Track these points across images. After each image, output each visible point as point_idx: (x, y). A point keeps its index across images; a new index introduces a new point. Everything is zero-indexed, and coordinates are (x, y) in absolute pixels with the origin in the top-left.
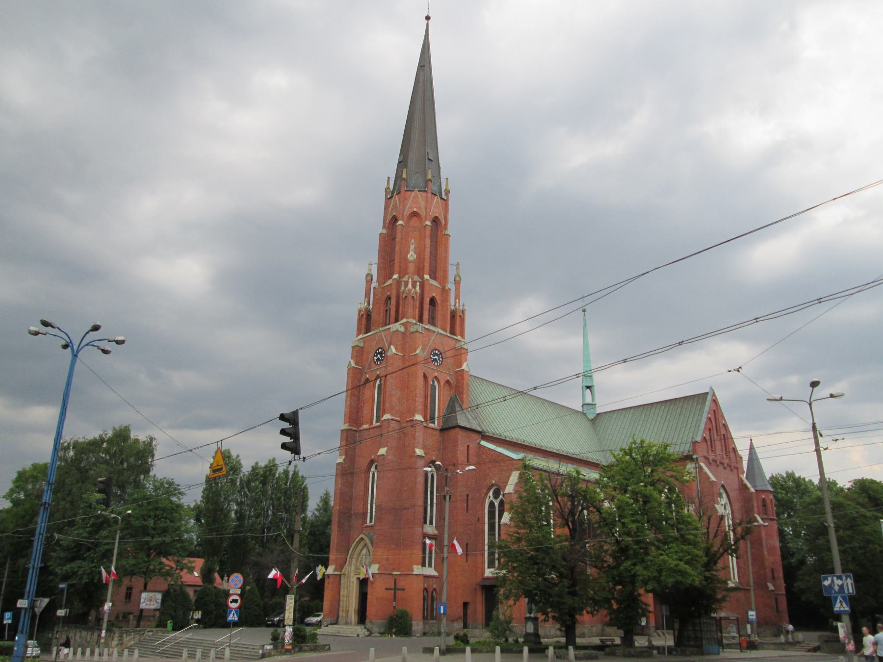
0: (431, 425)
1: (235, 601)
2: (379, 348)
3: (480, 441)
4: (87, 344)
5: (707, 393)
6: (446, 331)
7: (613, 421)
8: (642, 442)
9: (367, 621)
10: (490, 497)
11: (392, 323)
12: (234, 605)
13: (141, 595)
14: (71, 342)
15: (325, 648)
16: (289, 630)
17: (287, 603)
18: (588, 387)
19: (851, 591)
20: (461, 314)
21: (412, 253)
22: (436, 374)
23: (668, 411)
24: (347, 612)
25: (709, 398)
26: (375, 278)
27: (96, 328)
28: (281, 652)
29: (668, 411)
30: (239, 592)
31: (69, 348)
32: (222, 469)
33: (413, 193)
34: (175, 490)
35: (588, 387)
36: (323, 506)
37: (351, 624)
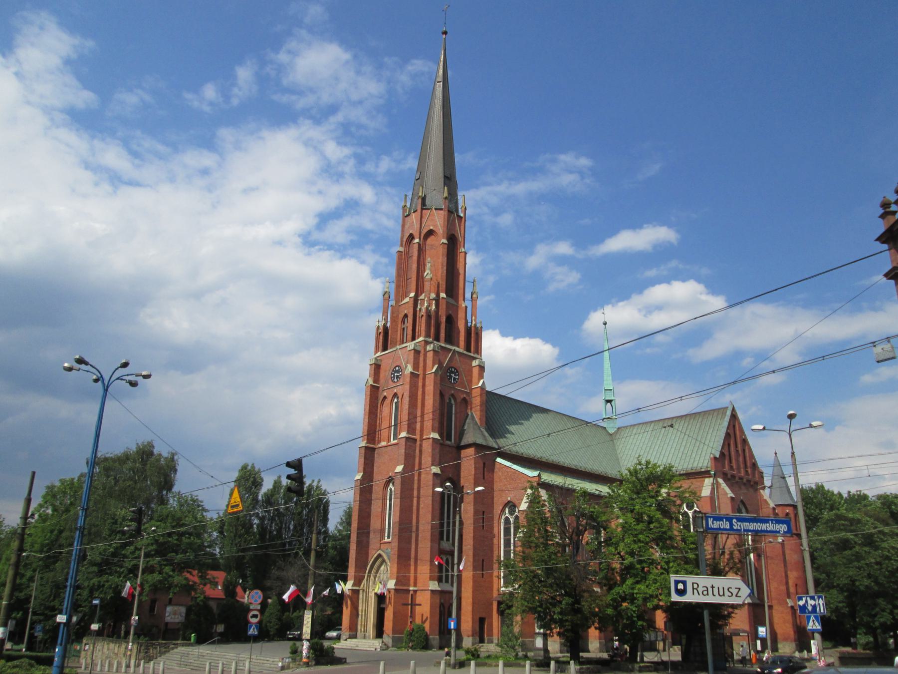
0: (448, 442)
1: (255, 616)
4: (118, 379)
8: (648, 463)
9: (385, 636)
11: (409, 341)
12: (254, 620)
13: (166, 609)
14: (102, 376)
15: (341, 661)
16: (306, 645)
17: (305, 618)
19: (822, 611)
21: (427, 271)
22: (453, 392)
26: (392, 297)
27: (125, 365)
28: (299, 665)
30: (259, 607)
31: (100, 382)
34: (199, 506)
35: (610, 401)
36: (346, 519)
37: (369, 638)
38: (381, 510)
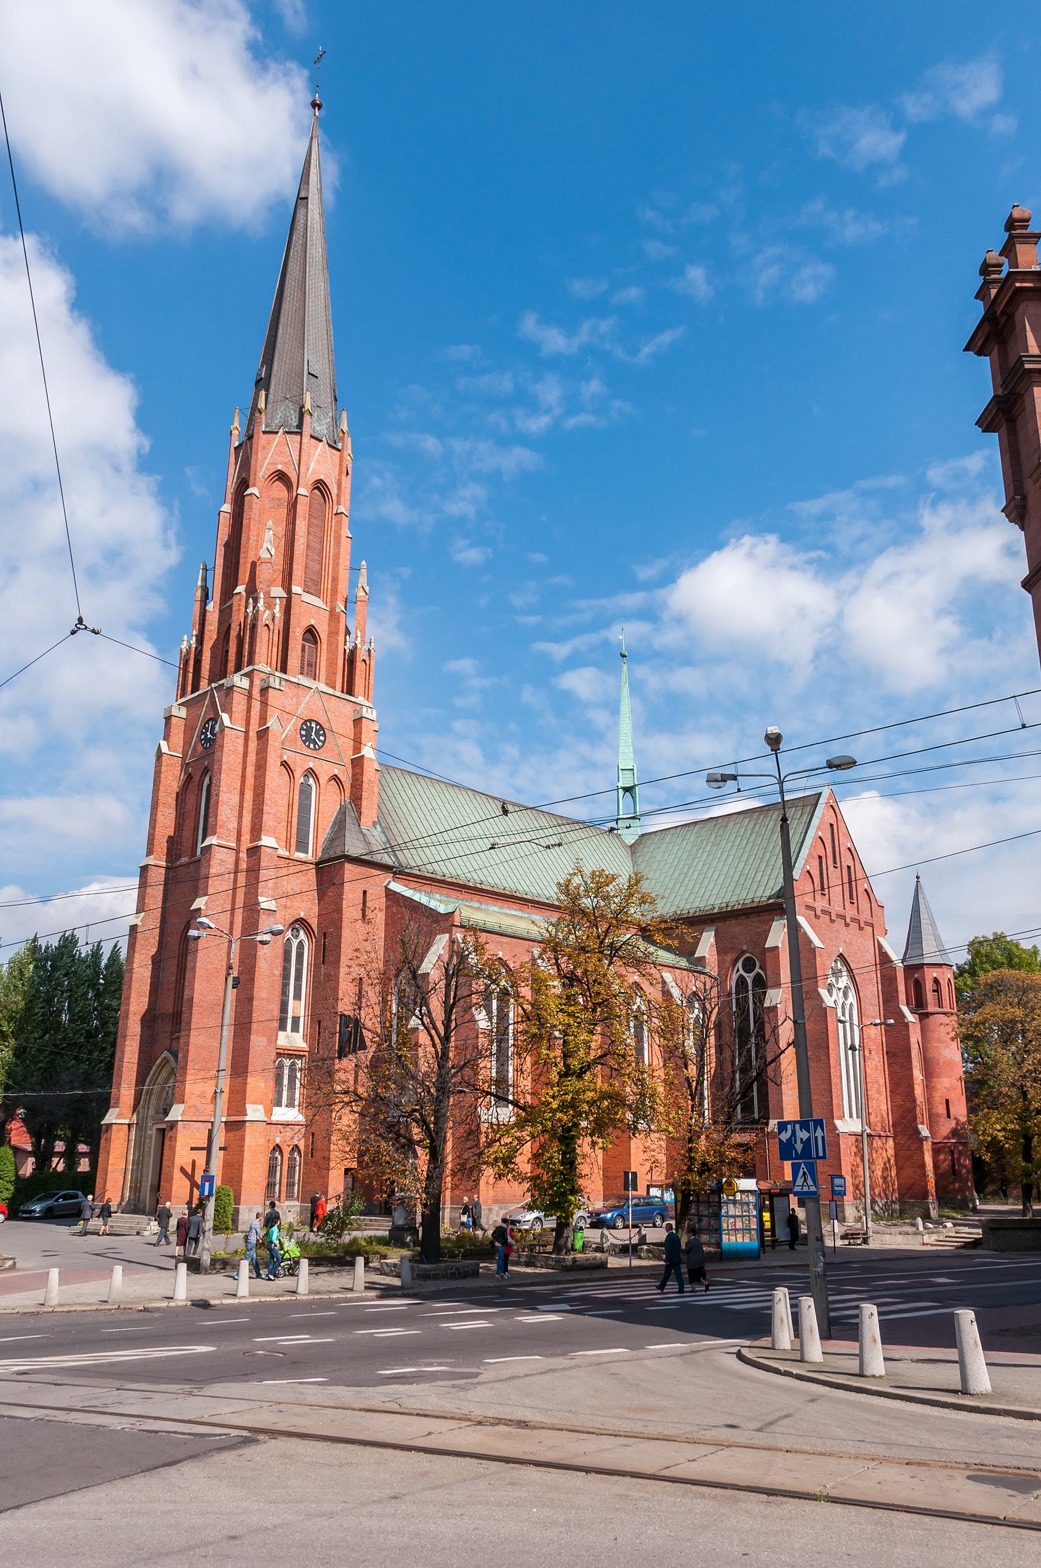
0: (301, 856)
6: (334, 688)
10: (738, 970)
22: (311, 765)
23: (755, 825)
29: (755, 825)
33: (277, 437)
38: (174, 979)
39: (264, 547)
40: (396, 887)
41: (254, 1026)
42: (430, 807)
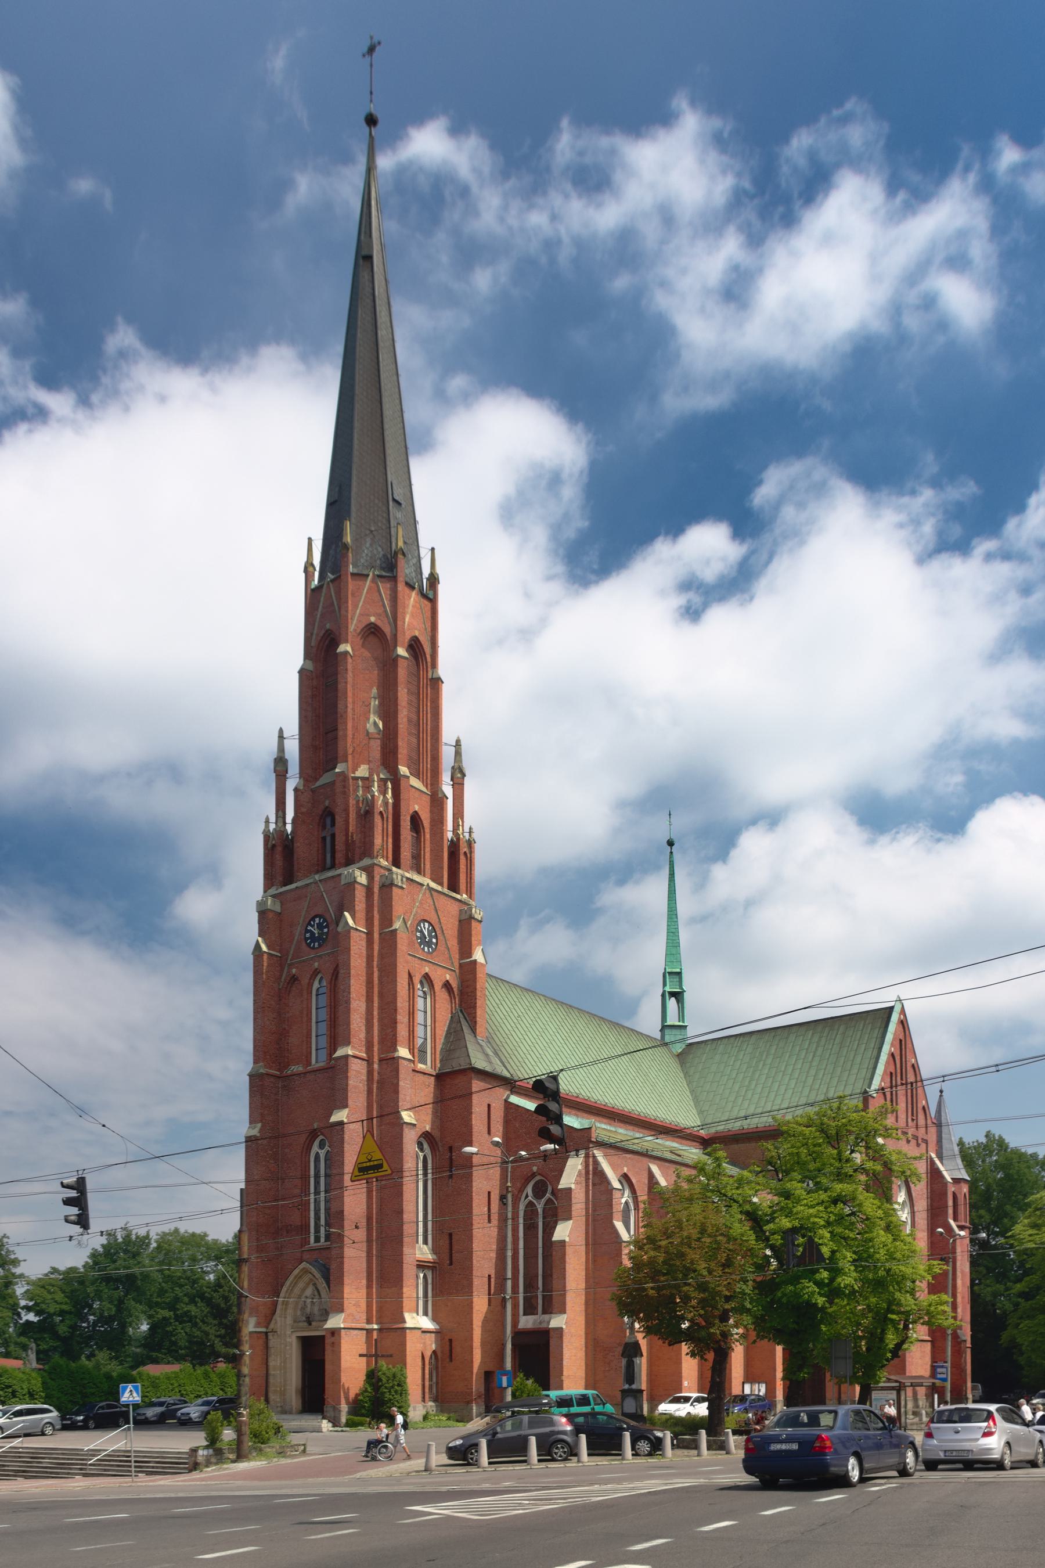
2: (316, 916)
3: (508, 1097)
5: (891, 1009)
6: (441, 884)
7: (718, 1057)
10: (527, 1196)
18: (673, 994)
20: (466, 850)
22: (427, 970)
23: (820, 1037)
24: (283, 1393)
25: (895, 1017)
32: (381, 1166)
35: (673, 994)
39: (371, 720)
40: (515, 1099)
41: (405, 1240)
42: (516, 1015)
